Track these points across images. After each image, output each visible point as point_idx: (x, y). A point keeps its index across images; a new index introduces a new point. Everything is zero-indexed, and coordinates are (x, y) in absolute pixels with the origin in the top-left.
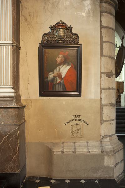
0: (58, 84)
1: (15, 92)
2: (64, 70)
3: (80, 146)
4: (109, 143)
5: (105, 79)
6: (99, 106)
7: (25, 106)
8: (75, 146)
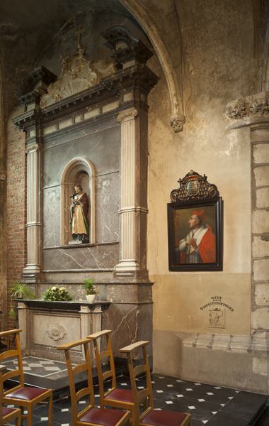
0: (192, 254)
1: (137, 266)
2: (199, 235)
3: (219, 340)
4: (265, 341)
5: (259, 243)
6: (248, 283)
7: (152, 284)
8: (213, 340)
